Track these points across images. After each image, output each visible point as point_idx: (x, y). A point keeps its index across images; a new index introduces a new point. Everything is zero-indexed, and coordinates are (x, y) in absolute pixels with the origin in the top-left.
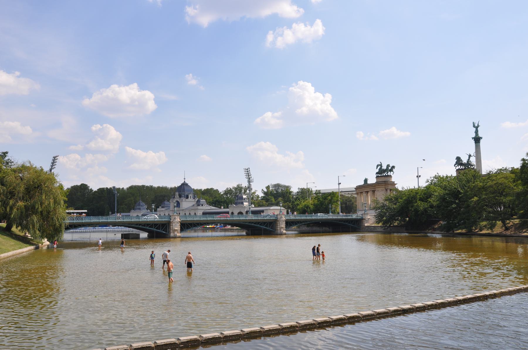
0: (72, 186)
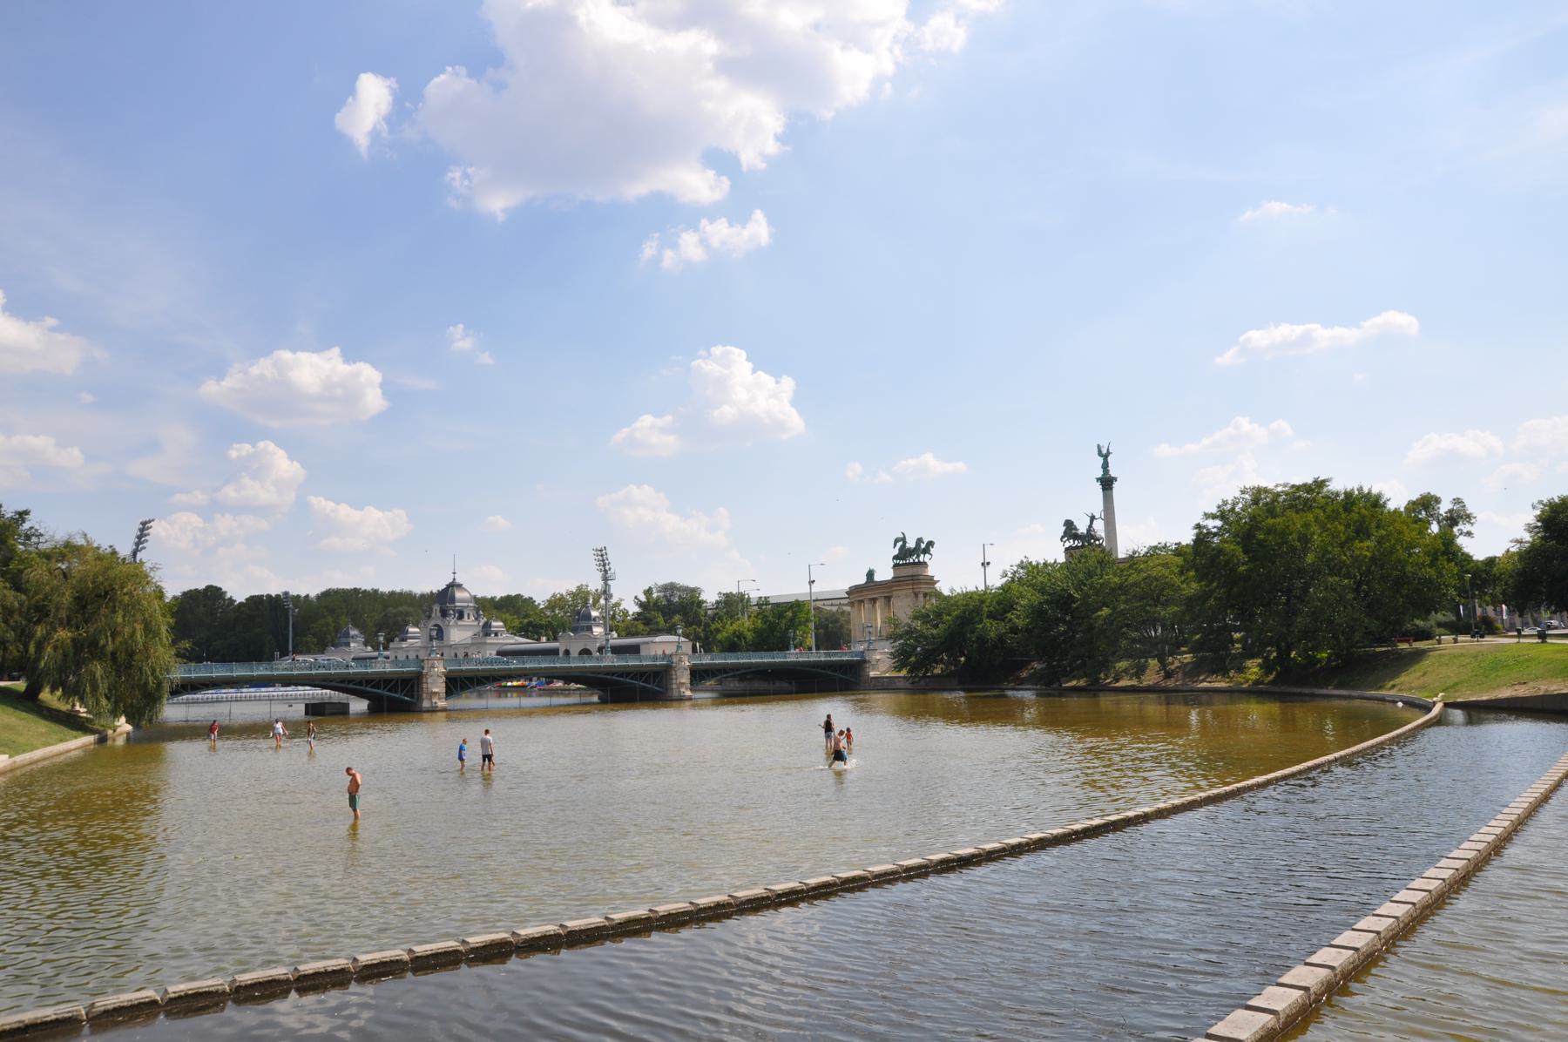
0: (184, 592)
